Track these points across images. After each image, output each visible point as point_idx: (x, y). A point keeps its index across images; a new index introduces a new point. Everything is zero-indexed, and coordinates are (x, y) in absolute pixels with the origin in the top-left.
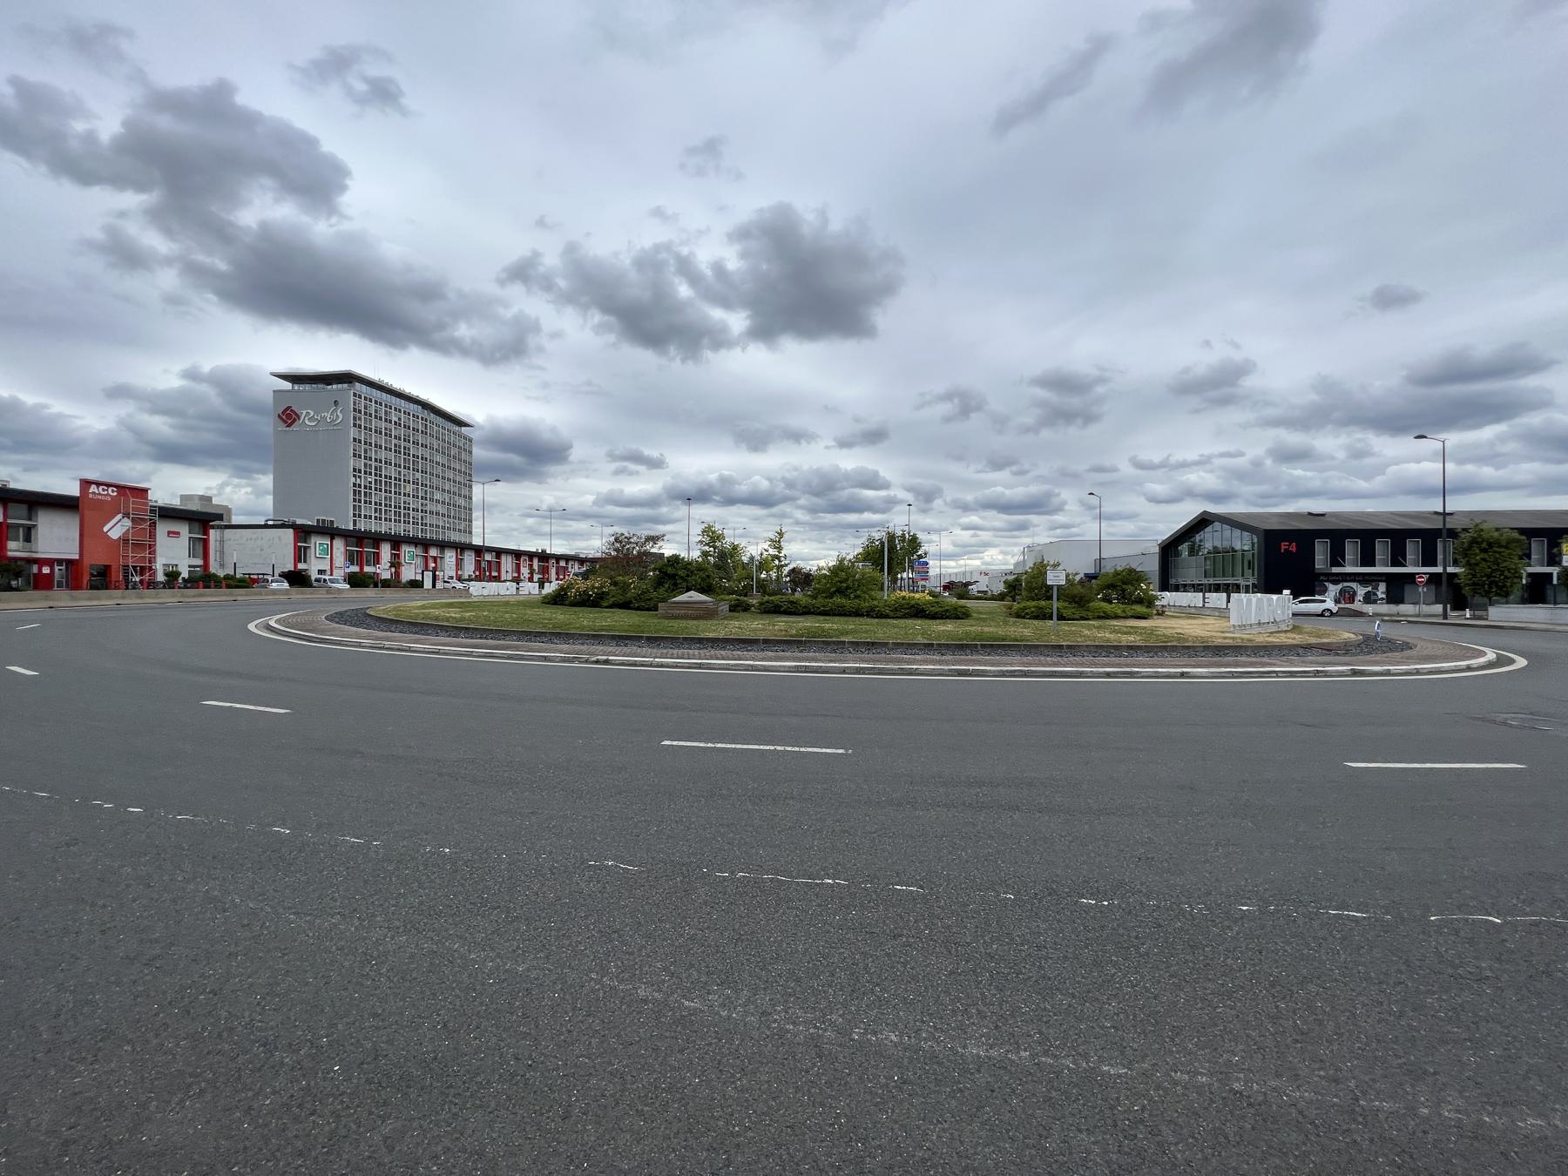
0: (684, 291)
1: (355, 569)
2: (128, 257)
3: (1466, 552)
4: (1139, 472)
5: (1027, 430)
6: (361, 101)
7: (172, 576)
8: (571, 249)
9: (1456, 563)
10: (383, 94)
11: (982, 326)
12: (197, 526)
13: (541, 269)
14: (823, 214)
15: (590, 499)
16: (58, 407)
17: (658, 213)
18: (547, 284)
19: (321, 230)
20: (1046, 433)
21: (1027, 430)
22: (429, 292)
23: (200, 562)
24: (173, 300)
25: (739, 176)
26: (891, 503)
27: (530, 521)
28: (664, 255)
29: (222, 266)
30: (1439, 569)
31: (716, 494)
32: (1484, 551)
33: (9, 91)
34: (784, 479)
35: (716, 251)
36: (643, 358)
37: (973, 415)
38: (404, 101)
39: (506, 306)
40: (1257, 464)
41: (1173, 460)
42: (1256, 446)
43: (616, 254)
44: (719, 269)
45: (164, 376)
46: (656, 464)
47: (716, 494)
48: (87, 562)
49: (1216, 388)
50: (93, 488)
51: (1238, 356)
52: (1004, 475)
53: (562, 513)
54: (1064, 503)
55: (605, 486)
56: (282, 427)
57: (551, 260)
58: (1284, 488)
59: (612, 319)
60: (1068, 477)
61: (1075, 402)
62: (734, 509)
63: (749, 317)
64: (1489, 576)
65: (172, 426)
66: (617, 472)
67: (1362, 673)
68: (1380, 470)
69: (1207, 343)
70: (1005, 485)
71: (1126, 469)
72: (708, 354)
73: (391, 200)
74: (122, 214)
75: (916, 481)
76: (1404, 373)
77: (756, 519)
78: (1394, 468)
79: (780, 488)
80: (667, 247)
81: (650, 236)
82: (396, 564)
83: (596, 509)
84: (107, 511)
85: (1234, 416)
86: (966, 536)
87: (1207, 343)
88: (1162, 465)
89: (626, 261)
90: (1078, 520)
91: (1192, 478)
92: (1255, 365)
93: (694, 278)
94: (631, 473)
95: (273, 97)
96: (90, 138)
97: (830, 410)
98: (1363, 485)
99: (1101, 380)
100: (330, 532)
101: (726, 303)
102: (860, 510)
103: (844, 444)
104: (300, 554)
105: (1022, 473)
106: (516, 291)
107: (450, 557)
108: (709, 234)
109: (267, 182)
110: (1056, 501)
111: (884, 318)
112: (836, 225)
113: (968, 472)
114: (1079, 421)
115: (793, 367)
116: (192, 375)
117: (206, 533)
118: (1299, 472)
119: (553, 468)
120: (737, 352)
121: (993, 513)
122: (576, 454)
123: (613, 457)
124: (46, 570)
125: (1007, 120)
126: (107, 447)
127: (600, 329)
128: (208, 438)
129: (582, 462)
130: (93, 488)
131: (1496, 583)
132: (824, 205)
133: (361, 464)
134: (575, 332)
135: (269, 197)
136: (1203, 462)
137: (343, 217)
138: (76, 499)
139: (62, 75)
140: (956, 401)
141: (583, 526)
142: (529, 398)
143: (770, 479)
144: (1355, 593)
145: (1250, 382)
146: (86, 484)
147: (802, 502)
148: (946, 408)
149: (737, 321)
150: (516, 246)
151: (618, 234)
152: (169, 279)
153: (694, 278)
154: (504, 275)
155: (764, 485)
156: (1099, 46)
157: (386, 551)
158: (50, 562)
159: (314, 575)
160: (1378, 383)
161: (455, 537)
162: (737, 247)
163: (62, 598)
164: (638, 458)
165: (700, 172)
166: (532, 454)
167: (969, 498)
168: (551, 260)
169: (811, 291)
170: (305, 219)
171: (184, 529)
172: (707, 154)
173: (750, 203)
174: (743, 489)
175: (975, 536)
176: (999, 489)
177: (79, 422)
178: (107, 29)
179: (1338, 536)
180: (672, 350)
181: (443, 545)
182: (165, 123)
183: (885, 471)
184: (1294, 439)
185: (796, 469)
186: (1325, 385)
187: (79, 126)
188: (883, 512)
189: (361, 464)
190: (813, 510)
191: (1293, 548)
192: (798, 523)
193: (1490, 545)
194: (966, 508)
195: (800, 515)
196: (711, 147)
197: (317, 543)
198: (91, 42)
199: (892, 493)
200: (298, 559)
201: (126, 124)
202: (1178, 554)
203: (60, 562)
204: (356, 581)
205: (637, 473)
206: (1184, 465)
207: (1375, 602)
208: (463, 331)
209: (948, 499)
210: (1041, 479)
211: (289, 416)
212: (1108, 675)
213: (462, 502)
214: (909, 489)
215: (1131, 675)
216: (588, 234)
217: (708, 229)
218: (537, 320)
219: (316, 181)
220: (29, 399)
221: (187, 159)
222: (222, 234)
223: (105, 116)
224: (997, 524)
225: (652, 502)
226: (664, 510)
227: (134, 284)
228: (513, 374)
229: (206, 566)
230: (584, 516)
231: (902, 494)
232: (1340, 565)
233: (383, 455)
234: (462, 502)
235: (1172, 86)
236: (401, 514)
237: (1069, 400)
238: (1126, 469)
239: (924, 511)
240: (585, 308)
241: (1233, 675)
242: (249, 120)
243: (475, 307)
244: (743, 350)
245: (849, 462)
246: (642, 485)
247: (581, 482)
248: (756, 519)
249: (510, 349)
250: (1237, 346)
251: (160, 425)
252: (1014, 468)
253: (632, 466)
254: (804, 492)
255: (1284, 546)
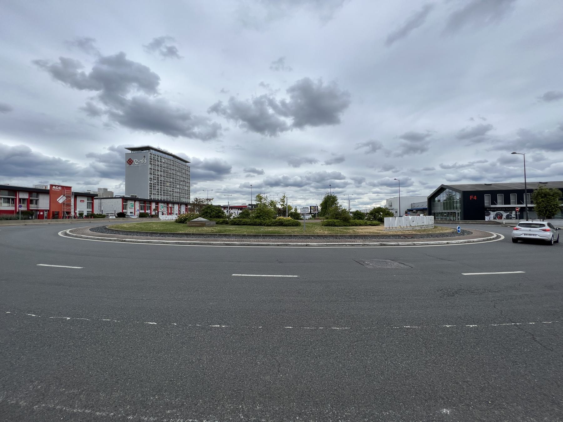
0: (271, 111)
1: (143, 211)
2: (93, 112)
3: (536, 198)
4: (443, 170)
5: (398, 155)
6: (165, 55)
7: (81, 215)
8: (232, 99)
9: (532, 203)
10: (172, 52)
11: (378, 118)
12: (90, 199)
13: (222, 107)
14: (320, 81)
15: (239, 185)
16: (72, 161)
17: (262, 84)
18: (224, 112)
19: (151, 99)
20: (406, 156)
21: (398, 155)
22: (185, 117)
23: (91, 210)
24: (106, 125)
25: (291, 69)
26: (345, 185)
27: (218, 194)
28: (263, 100)
29: (121, 113)
30: (524, 205)
31: (282, 183)
32: (542, 197)
33: (59, 61)
34: (306, 177)
35: (283, 97)
36: (257, 136)
37: (377, 151)
38: (178, 53)
39: (210, 120)
40: (493, 165)
41: (457, 165)
42: (493, 158)
43: (247, 100)
44: (283, 103)
45: (103, 149)
46: (260, 173)
47: (282, 183)
48: (52, 210)
49: (477, 136)
50: (54, 187)
51: (484, 123)
52: (390, 173)
53: (227, 192)
54: (413, 182)
55: (243, 181)
56: (128, 165)
57: (225, 103)
58: (505, 174)
59: (245, 123)
60: (415, 172)
61: (418, 144)
62: (288, 188)
63: (294, 119)
64: (545, 208)
65: (106, 166)
66: (247, 176)
67: (384, 245)
68: (548, 165)
69: (472, 119)
70: (389, 176)
71: (438, 169)
72: (279, 133)
73: (173, 88)
74: (92, 99)
75: (355, 176)
76: (559, 126)
77: (296, 191)
78: (554, 165)
79: (305, 180)
80: (265, 96)
81: (260, 93)
82: (157, 209)
83: (240, 189)
84: (58, 194)
85: (483, 147)
86: (374, 196)
87: (472, 119)
88: (454, 167)
89: (251, 102)
90: (418, 189)
91: (466, 171)
92: (492, 126)
93: (274, 107)
94: (252, 176)
95: (137, 56)
96: (83, 74)
97: (323, 151)
98: (539, 172)
99: (428, 135)
100: (134, 199)
101: (285, 115)
102: (334, 187)
103: (328, 163)
104: (124, 207)
105: (396, 172)
106: (214, 115)
107: (176, 207)
108: (280, 90)
109: (135, 84)
110: (409, 182)
111: (343, 116)
112: (325, 84)
113: (375, 172)
114: (419, 151)
115: (310, 136)
116: (112, 149)
117: (93, 201)
118: (511, 168)
119: (225, 176)
120: (289, 132)
121: (385, 187)
122: (233, 170)
123: (245, 171)
124: (42, 213)
125: (391, 40)
126: (86, 174)
127: (242, 126)
128: (116, 169)
129: (235, 173)
130: (54, 187)
131: (549, 210)
132: (320, 77)
133: (152, 177)
134: (233, 128)
135: (136, 90)
136: (470, 165)
137: (160, 94)
138: (48, 190)
139: (75, 55)
140: (371, 146)
141: (235, 195)
142: (217, 151)
143: (301, 177)
144: (502, 215)
145: (489, 133)
146: (52, 186)
147: (313, 185)
148: (366, 148)
149: (289, 121)
150: (213, 101)
151: (247, 95)
152: (105, 118)
153: (274, 107)
154: (210, 110)
155: (299, 179)
156: (427, 9)
157: (153, 206)
158: (43, 211)
159: (129, 214)
160: (547, 131)
161: (184, 200)
162: (290, 95)
163: (45, 222)
164: (254, 171)
165: (277, 69)
166: (217, 171)
167: (376, 181)
168: (225, 103)
169: (316, 108)
170: (147, 96)
171: (85, 199)
172: (280, 63)
173: (295, 78)
174: (291, 181)
175: (378, 196)
176: (387, 178)
177: (78, 166)
178: (88, 40)
179: (494, 193)
180: (266, 132)
181: (174, 203)
182: (105, 68)
183: (343, 173)
184: (508, 154)
185: (310, 173)
186: (523, 132)
187: (79, 71)
188: (342, 187)
189: (152, 177)
190: (317, 188)
191: (475, 198)
192: (311, 192)
193: (545, 195)
194: (374, 185)
195: (312, 190)
196: (281, 60)
197: (130, 203)
198: (84, 44)
199: (346, 181)
200: (123, 208)
201: (93, 69)
202: (434, 201)
203: (46, 210)
204: (142, 216)
205: (254, 176)
206: (462, 167)
207: (511, 219)
208: (196, 130)
209: (367, 182)
210: (404, 174)
211: (130, 162)
212: (278, 245)
213: (186, 188)
214: (353, 179)
215: (287, 245)
216: (238, 94)
217: (279, 90)
218: (220, 124)
219: (149, 82)
220: (64, 159)
221: (112, 79)
222: (121, 103)
223: (87, 67)
224: (386, 191)
225: (259, 186)
226: (263, 189)
227: (96, 121)
228: (213, 143)
229: (93, 211)
230: (236, 192)
231: (350, 181)
232: (495, 204)
233: (159, 173)
234: (186, 188)
235: (457, 21)
236: (165, 193)
237: (415, 144)
238: (438, 169)
239: (358, 187)
240: (236, 119)
241: (131, 242)
242: (130, 64)
243: (200, 122)
244: (291, 131)
245: (330, 170)
246: (256, 180)
247: (234, 180)
248: (296, 191)
249: (212, 135)
250: (484, 119)
251: (102, 166)
252: (393, 170)
253: (252, 174)
254: (313, 181)
255: (471, 197)
